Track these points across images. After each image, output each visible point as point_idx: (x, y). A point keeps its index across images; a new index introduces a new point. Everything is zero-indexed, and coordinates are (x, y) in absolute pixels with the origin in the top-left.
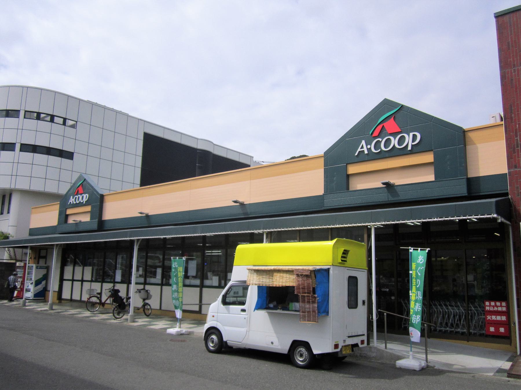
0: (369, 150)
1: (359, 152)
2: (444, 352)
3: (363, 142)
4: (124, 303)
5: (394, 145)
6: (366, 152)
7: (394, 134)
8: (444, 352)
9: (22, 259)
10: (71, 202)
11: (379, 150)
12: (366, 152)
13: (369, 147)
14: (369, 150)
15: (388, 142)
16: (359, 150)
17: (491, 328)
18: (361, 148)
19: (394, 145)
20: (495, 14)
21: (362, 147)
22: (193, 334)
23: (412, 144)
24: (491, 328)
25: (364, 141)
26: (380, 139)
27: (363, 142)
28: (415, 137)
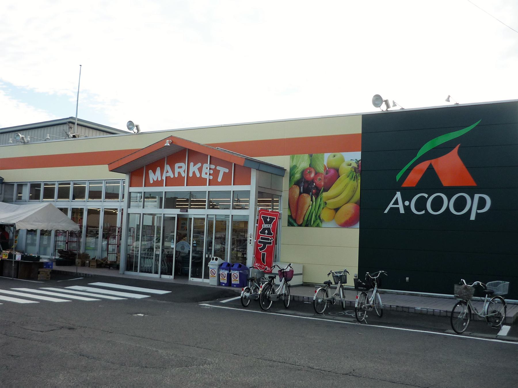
0: (407, 209)
1: (391, 208)
2: (74, 251)
3: (398, 195)
4: (463, 279)
5: (448, 208)
6: (402, 211)
7: (450, 192)
8: (74, 251)
9: (303, 300)
10: (354, 316)
11: (423, 212)
12: (402, 211)
13: (407, 203)
14: (407, 209)
15: (437, 204)
16: (391, 205)
17: (408, 278)
18: (394, 204)
19: (448, 208)
20: (139, 125)
21: (396, 203)
22: (84, 253)
23: (477, 212)
24: (408, 278)
25: (399, 192)
26: (426, 196)
27: (398, 195)
28: (482, 203)
